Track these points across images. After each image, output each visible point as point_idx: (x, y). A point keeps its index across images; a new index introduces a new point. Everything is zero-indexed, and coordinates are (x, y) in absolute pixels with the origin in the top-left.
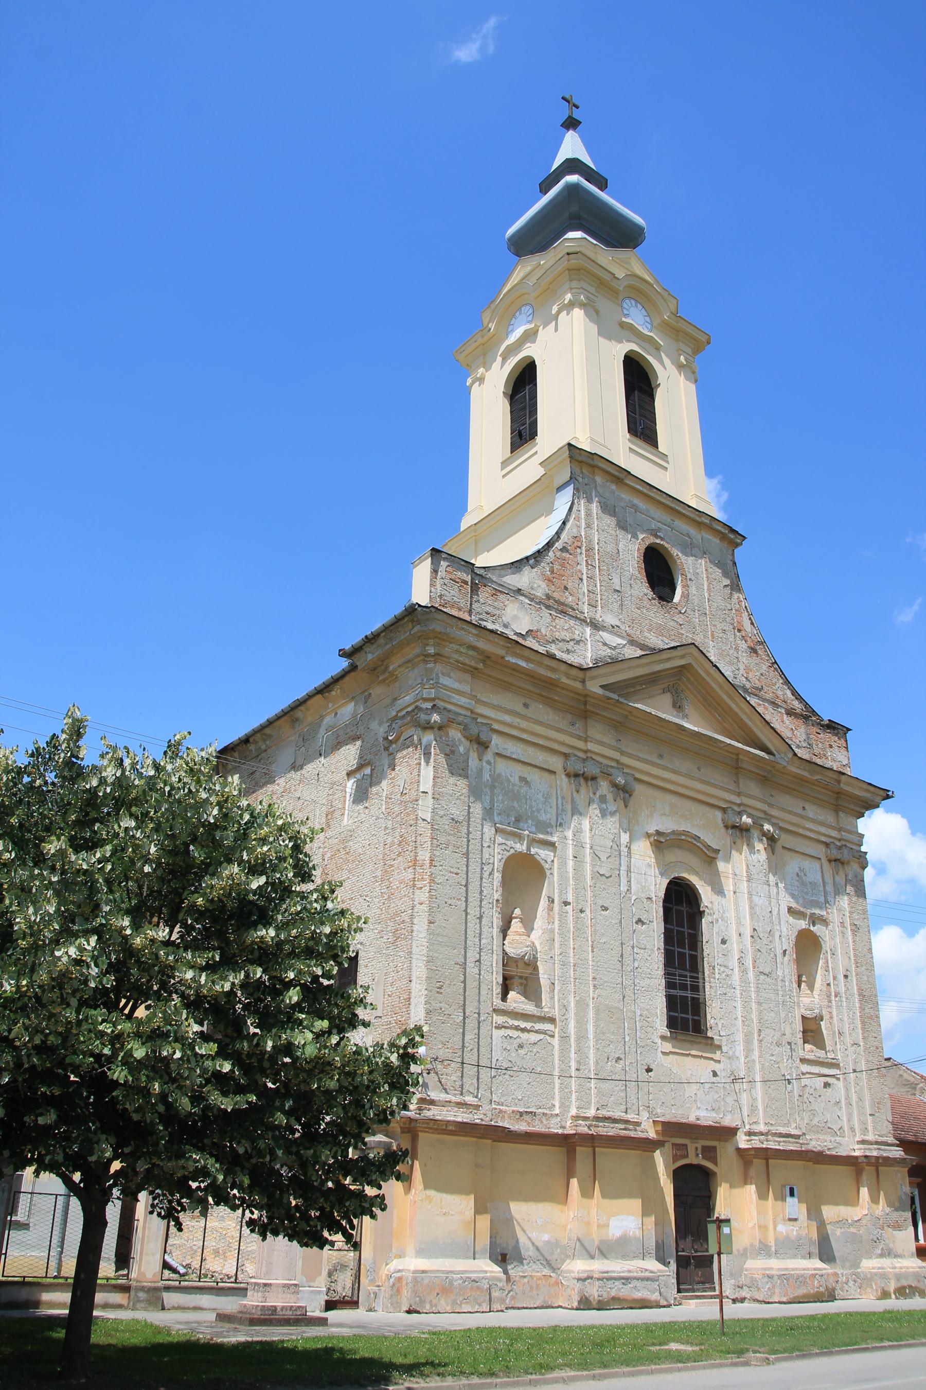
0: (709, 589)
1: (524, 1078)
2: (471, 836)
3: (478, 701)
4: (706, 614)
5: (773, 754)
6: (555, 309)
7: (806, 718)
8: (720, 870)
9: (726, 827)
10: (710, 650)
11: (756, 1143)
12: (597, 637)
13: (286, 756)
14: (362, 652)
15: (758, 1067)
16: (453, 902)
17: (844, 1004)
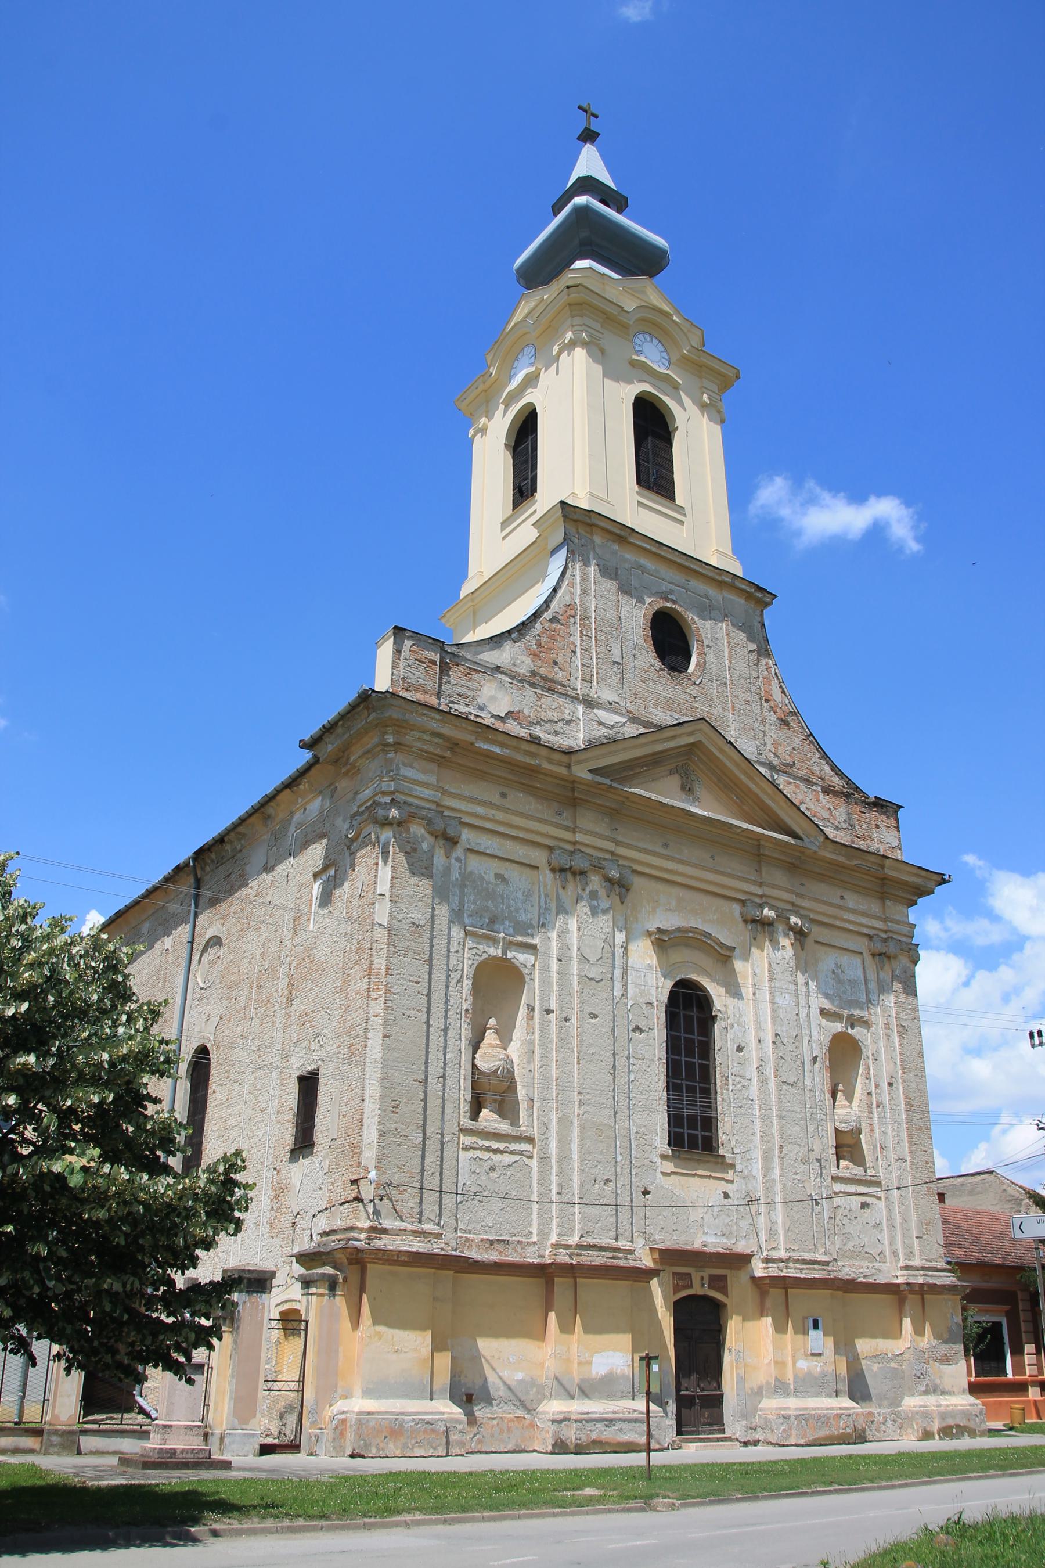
0: (730, 656)
1: (496, 1204)
2: (435, 942)
3: (445, 792)
4: (727, 685)
5: (801, 839)
6: (556, 349)
7: (847, 796)
8: (737, 970)
9: (745, 921)
10: (730, 724)
11: (774, 1270)
12: (591, 716)
13: (259, 857)
14: (323, 742)
15: (778, 1187)
16: (412, 1013)
17: (888, 1115)
